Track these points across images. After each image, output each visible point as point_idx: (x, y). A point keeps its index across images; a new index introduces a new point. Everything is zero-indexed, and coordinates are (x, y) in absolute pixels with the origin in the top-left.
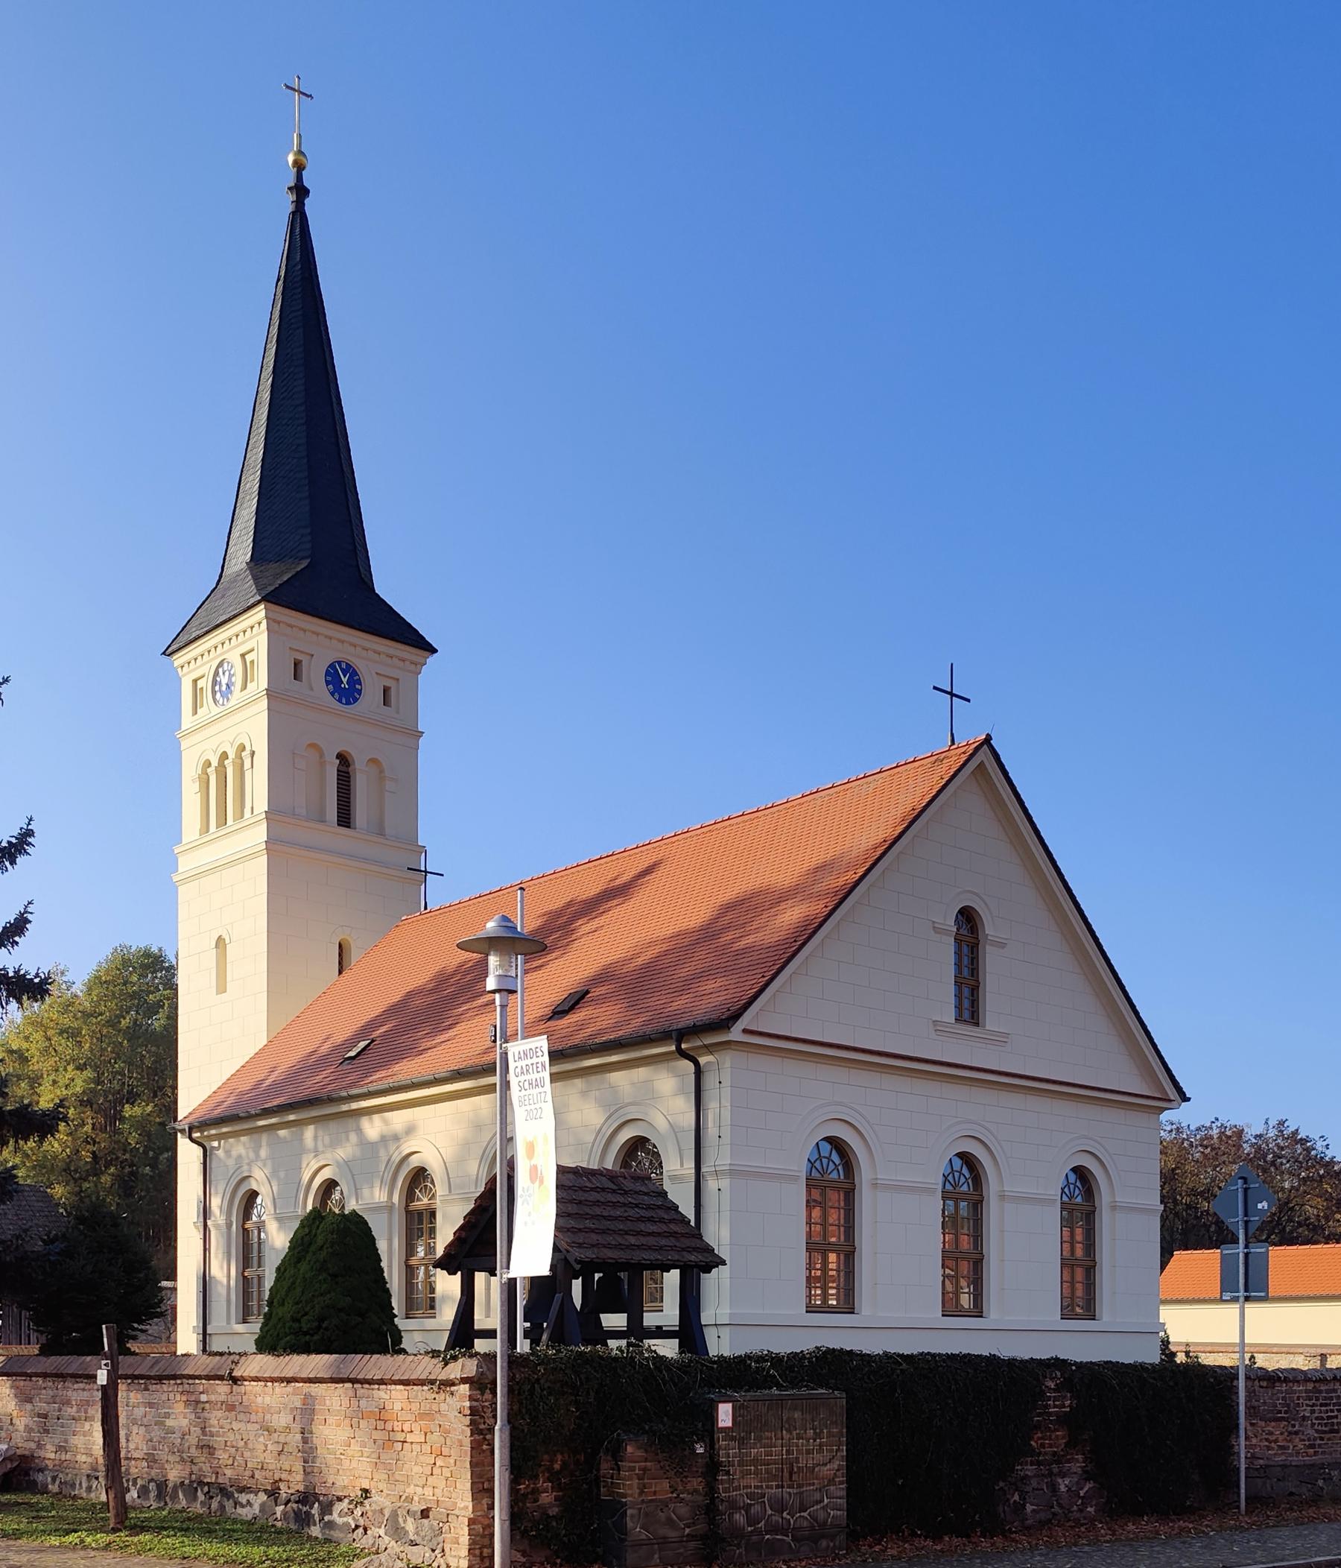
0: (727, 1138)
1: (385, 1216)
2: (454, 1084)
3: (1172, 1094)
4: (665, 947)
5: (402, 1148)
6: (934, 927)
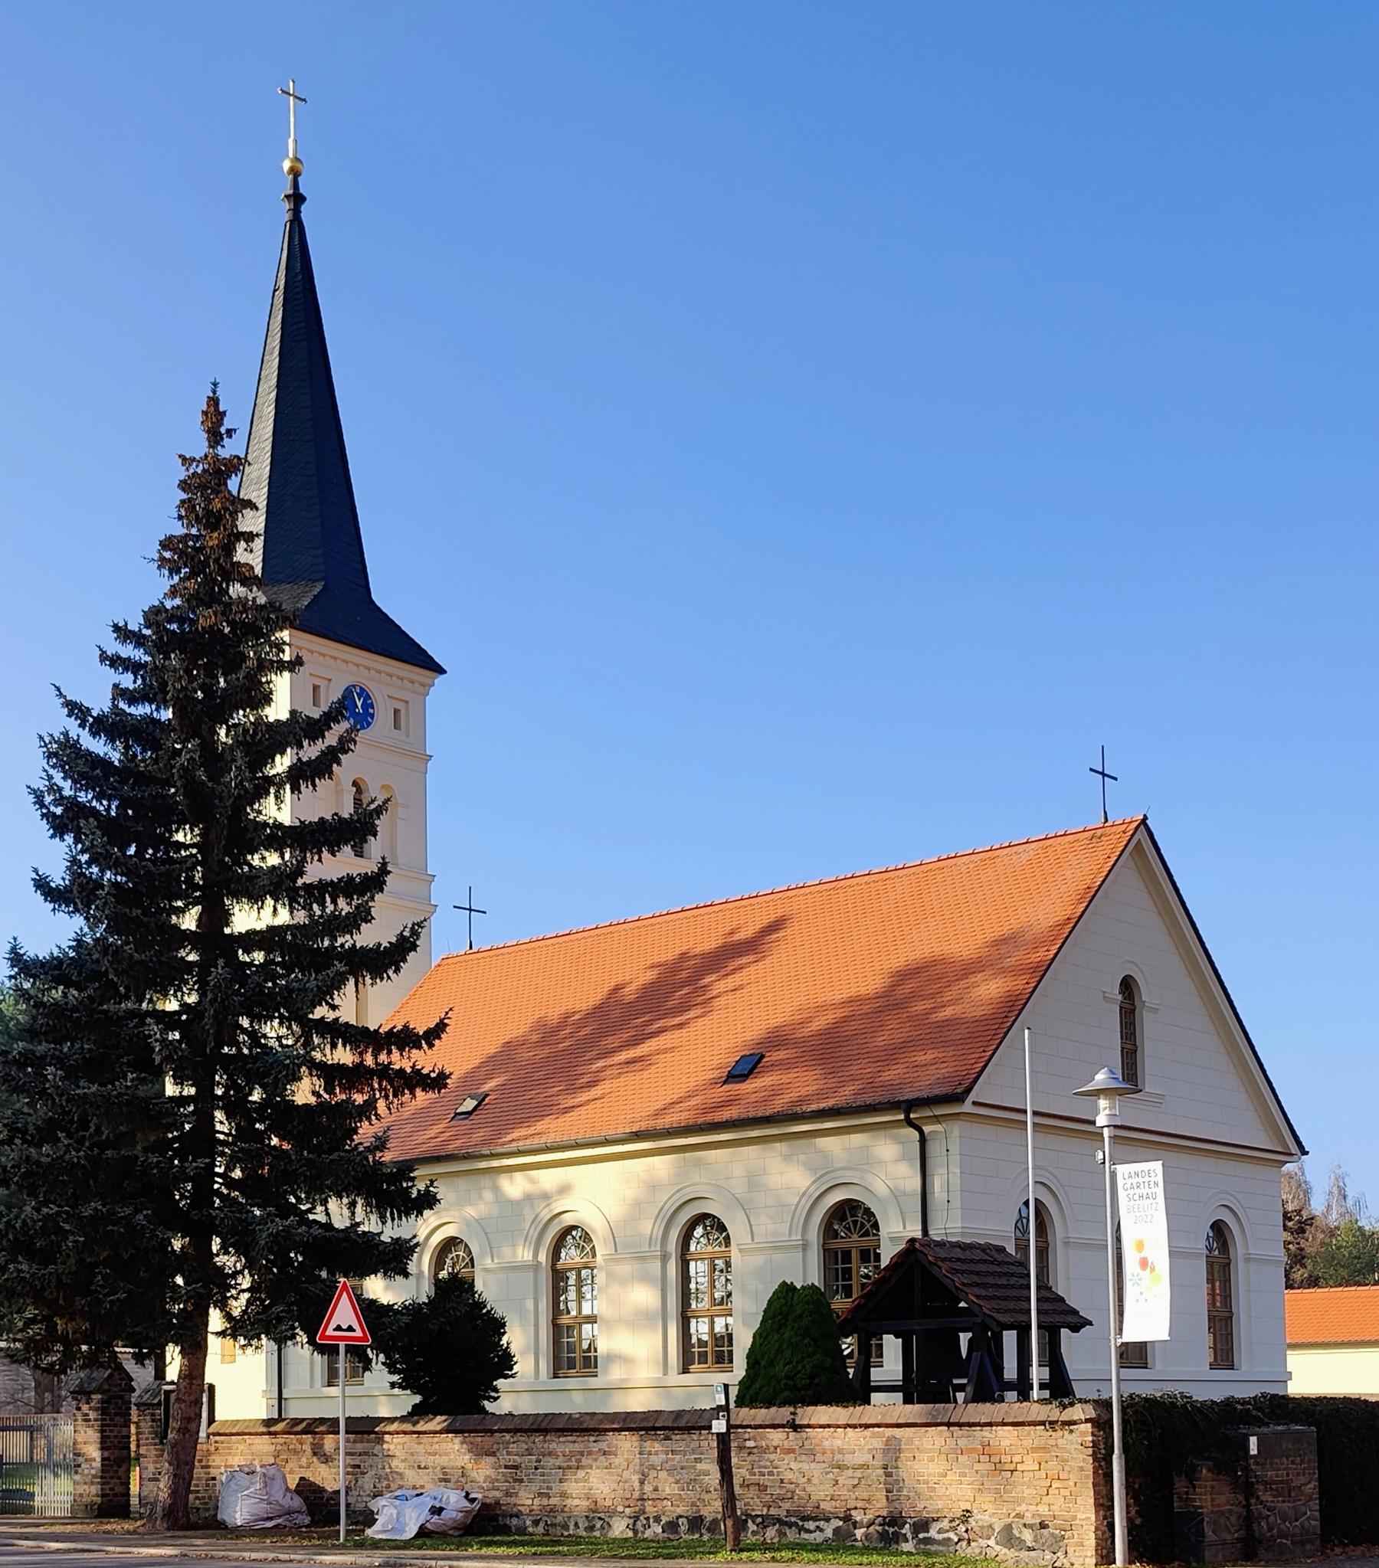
3: (1294, 1149)
4: (839, 1013)
5: (554, 1205)
6: (1104, 997)
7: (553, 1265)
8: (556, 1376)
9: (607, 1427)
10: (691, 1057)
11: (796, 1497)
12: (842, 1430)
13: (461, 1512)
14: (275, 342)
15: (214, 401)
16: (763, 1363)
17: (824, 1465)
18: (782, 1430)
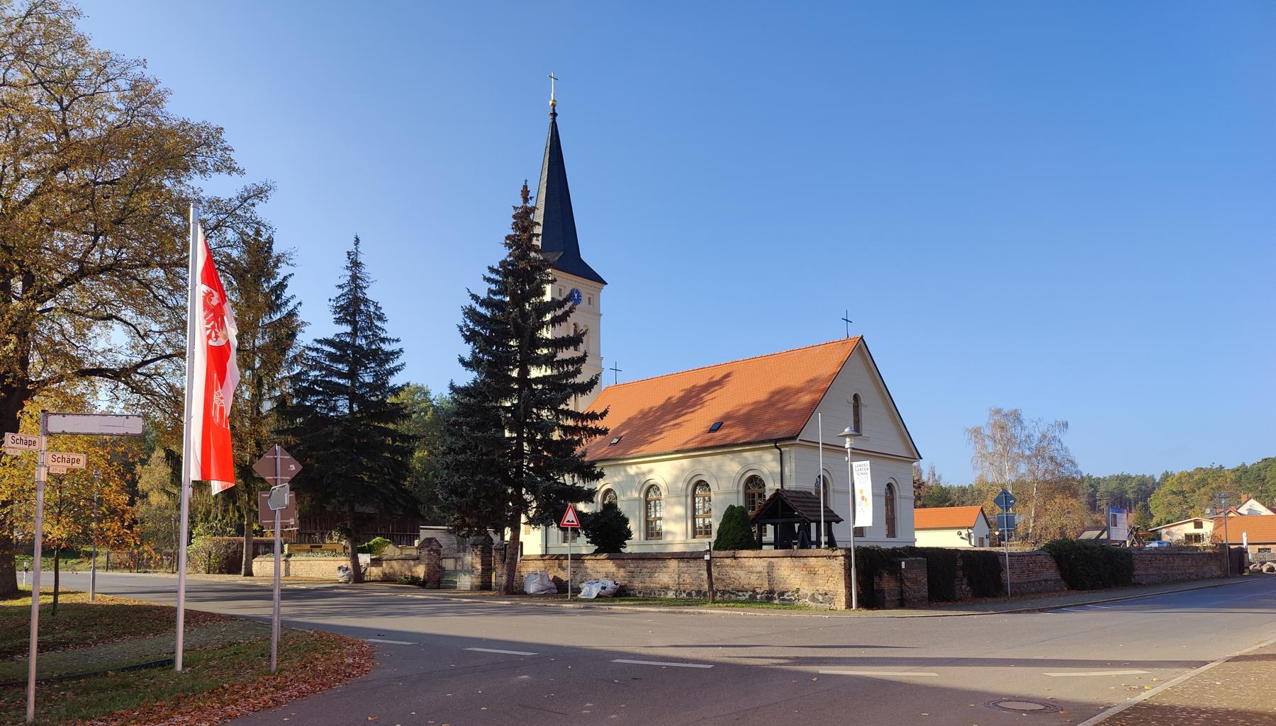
0: (793, 476)
1: (638, 502)
3: (917, 457)
8: (647, 539)
14: (546, 166)
15: (525, 187)
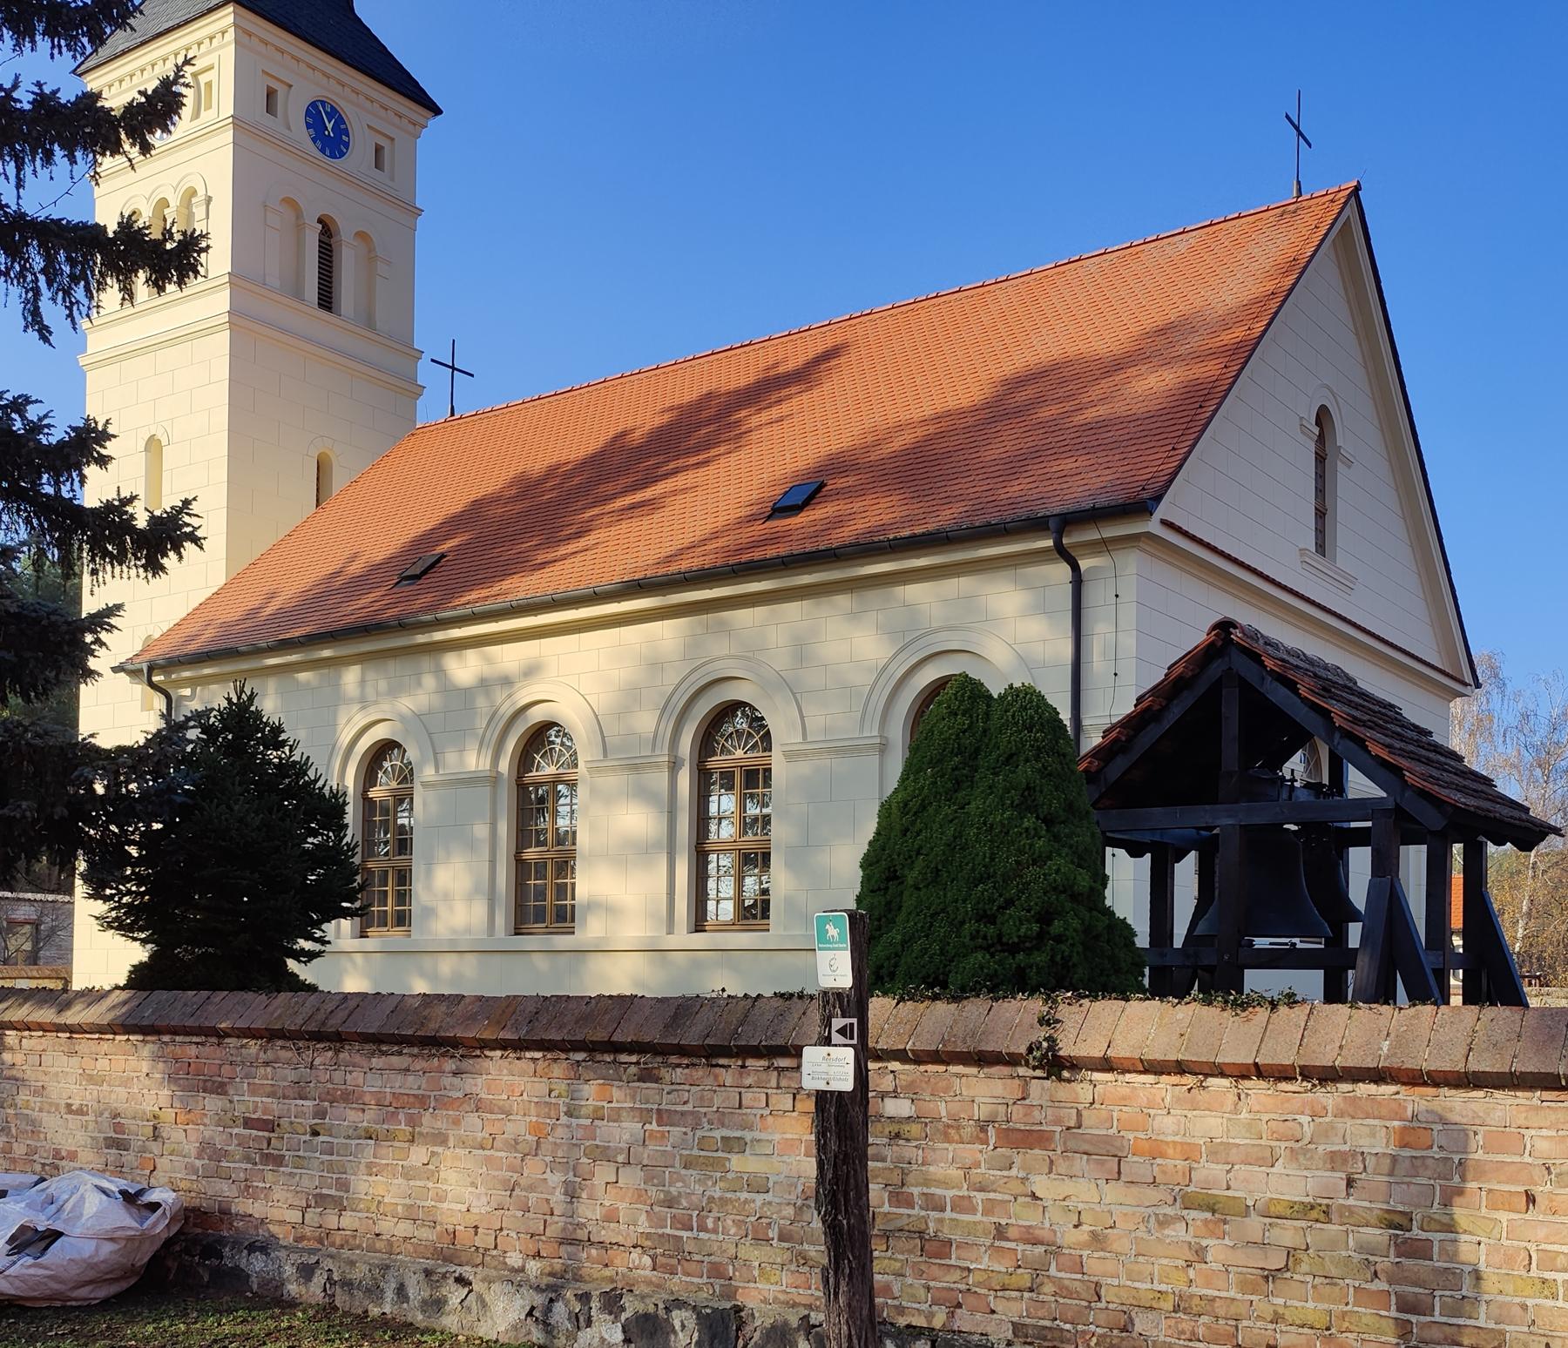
1: (486, 791)
2: (581, 610)
3: (1468, 678)
5: (517, 696)
7: (520, 777)
9: (487, 1035)
10: (720, 494)
11: (1049, 1288)
12: (1225, 1082)
13: (111, 1239)
16: (912, 876)
17: (1153, 1195)
18: (1006, 1070)
